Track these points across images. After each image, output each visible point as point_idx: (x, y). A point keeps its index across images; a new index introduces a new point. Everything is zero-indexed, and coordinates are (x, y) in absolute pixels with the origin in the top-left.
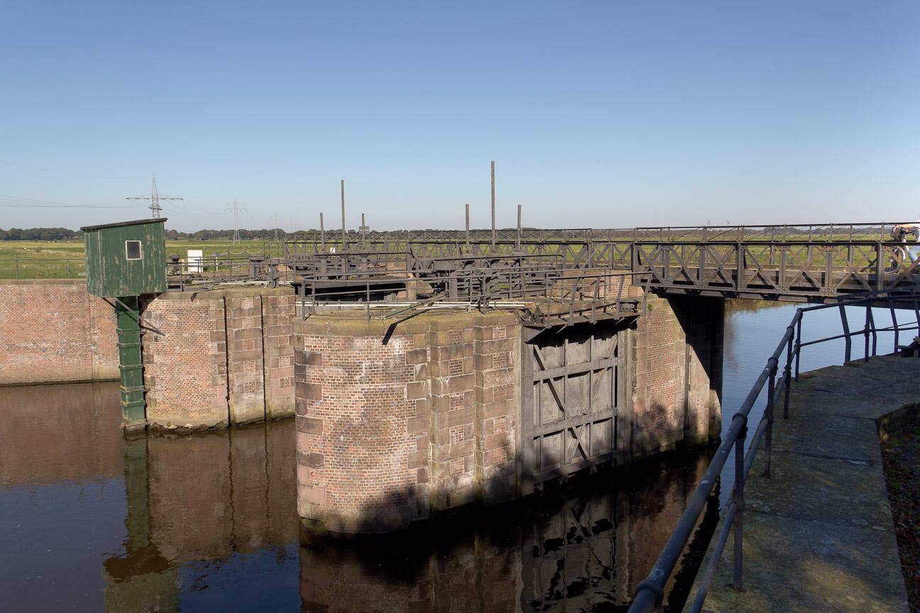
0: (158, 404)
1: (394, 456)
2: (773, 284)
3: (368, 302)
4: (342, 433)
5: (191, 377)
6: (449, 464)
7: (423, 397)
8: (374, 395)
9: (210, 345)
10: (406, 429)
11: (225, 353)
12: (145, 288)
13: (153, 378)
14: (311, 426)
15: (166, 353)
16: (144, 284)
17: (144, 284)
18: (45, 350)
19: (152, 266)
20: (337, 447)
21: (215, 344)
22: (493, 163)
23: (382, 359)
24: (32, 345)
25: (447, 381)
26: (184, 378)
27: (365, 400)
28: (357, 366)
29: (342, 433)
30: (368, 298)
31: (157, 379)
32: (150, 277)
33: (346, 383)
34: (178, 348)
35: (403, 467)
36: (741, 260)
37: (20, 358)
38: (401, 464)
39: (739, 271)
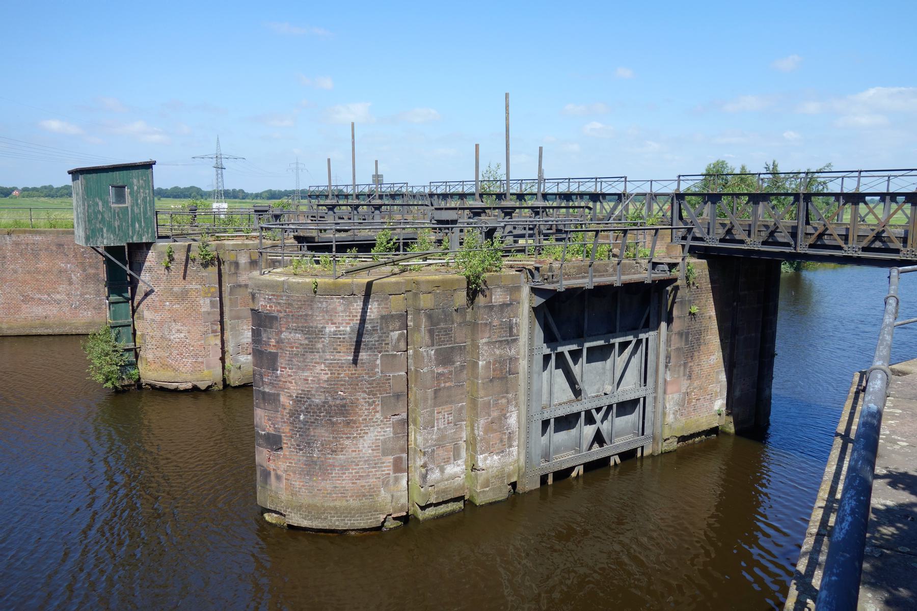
0: (149, 364)
1: (364, 440)
2: (841, 243)
3: (334, 253)
4: (301, 411)
5: (182, 335)
6: (433, 451)
7: (401, 371)
8: (339, 367)
9: (201, 302)
10: (379, 408)
11: (219, 310)
12: (132, 238)
13: (143, 335)
14: (271, 400)
15: (156, 311)
16: (131, 233)
17: (131, 233)
18: (58, 302)
19: (140, 213)
20: (296, 428)
21: (208, 301)
22: (507, 95)
23: (349, 324)
24: (46, 296)
25: (433, 352)
26: (175, 337)
27: (329, 372)
28: (319, 331)
29: (301, 411)
30: (334, 249)
31: (147, 337)
32: (137, 225)
33: (307, 352)
34: (168, 303)
35: (375, 454)
36: (802, 214)
37: (35, 309)
38: (373, 450)
39: (800, 227)
